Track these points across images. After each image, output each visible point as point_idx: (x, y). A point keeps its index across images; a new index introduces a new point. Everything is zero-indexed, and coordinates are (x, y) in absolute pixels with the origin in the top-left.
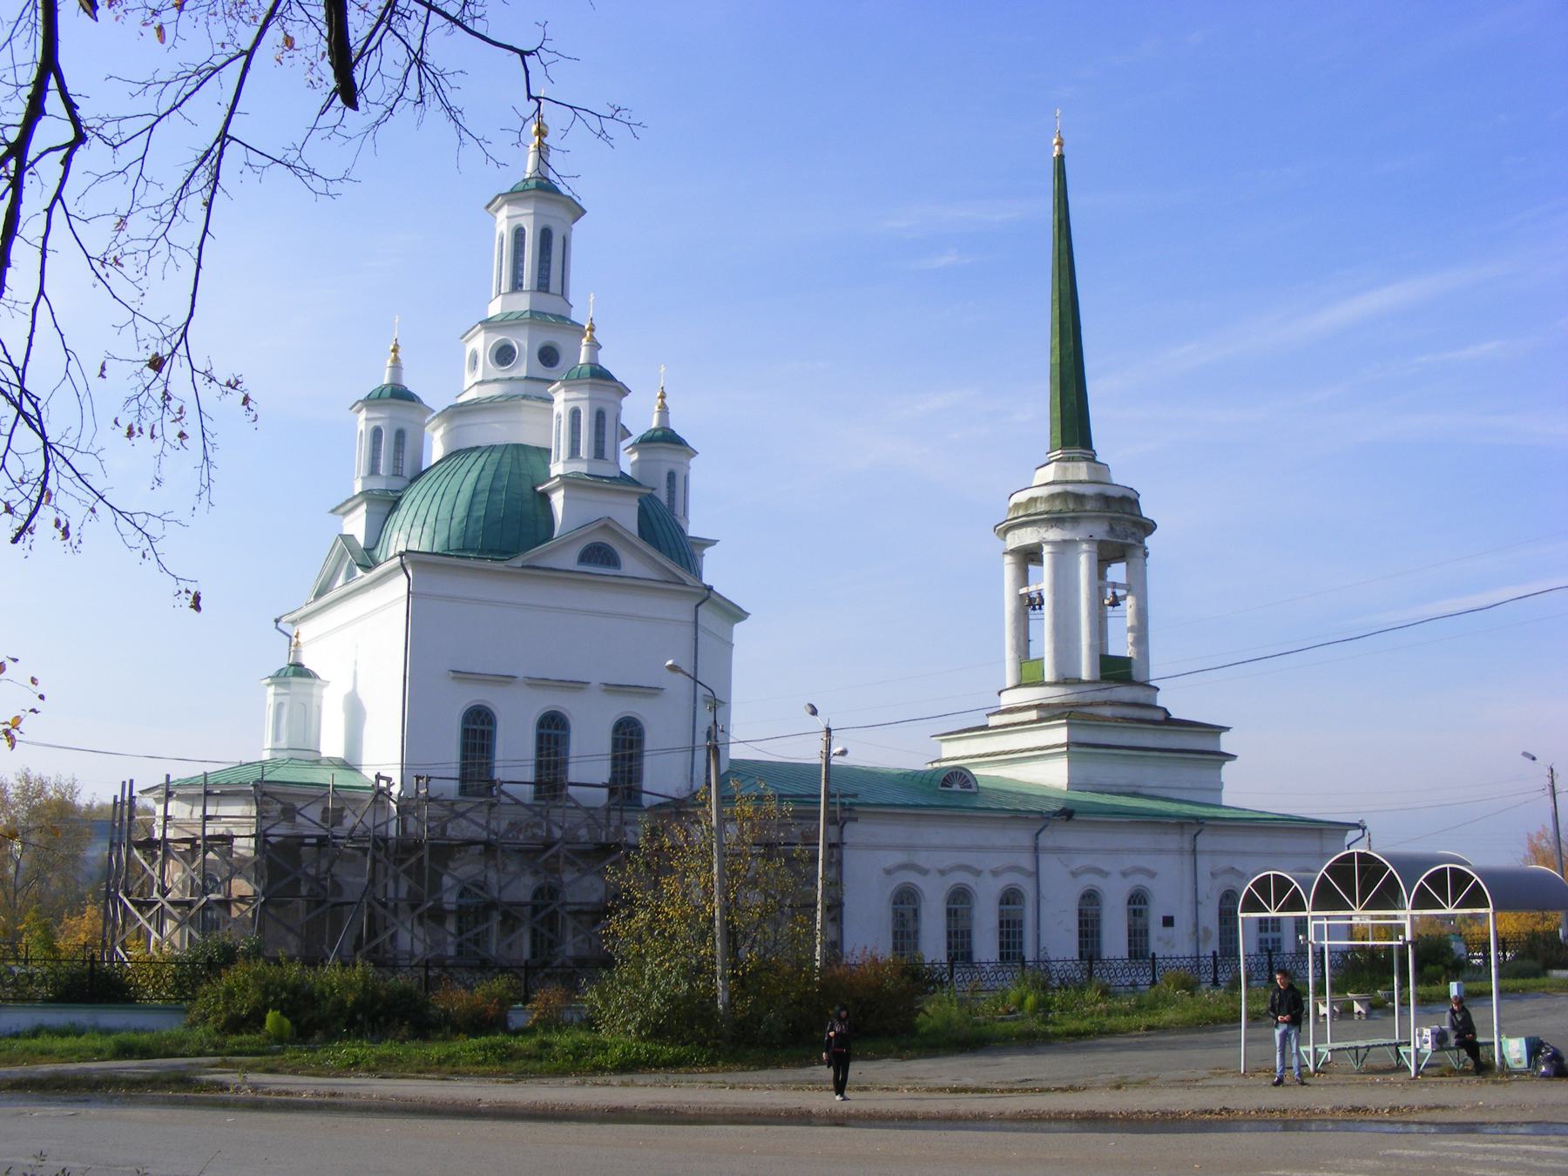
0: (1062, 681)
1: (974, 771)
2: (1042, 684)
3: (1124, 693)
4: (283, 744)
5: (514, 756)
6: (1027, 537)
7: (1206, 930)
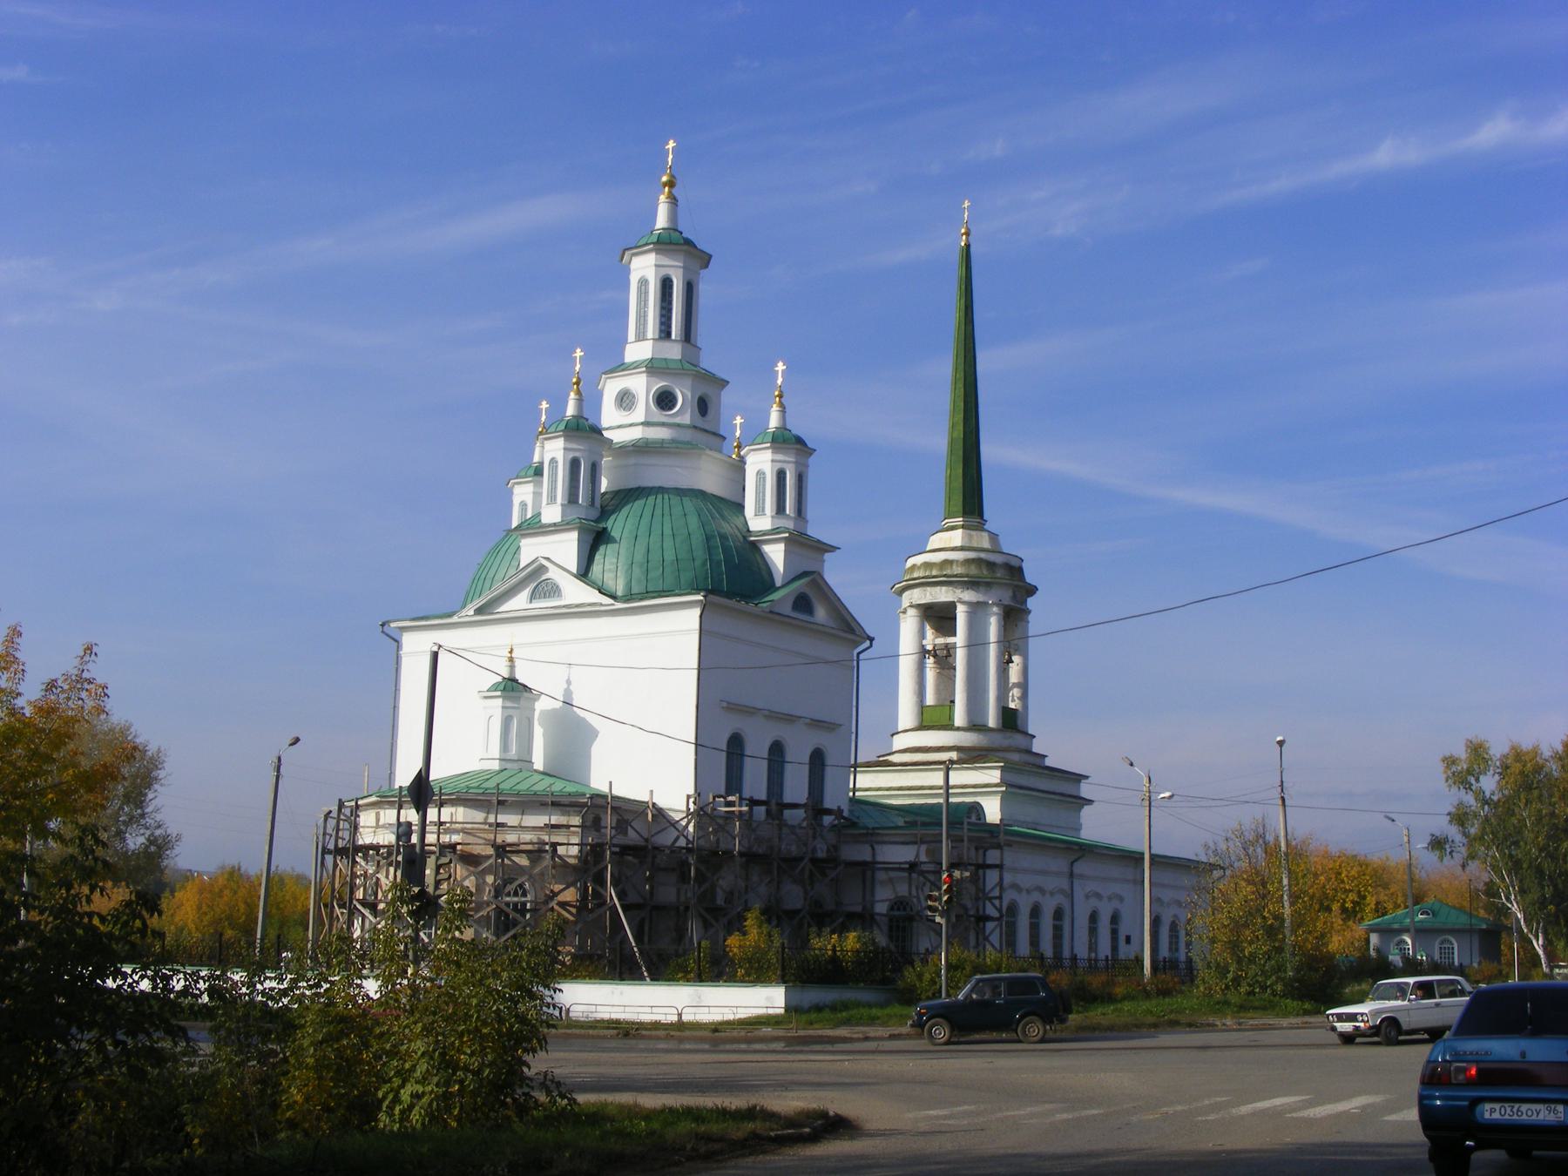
1: (535, 788)
2: (949, 726)
3: (1018, 740)
5: (755, 780)
6: (942, 595)
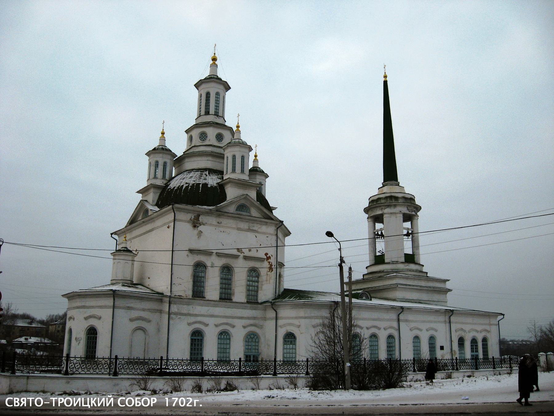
3: (412, 266)
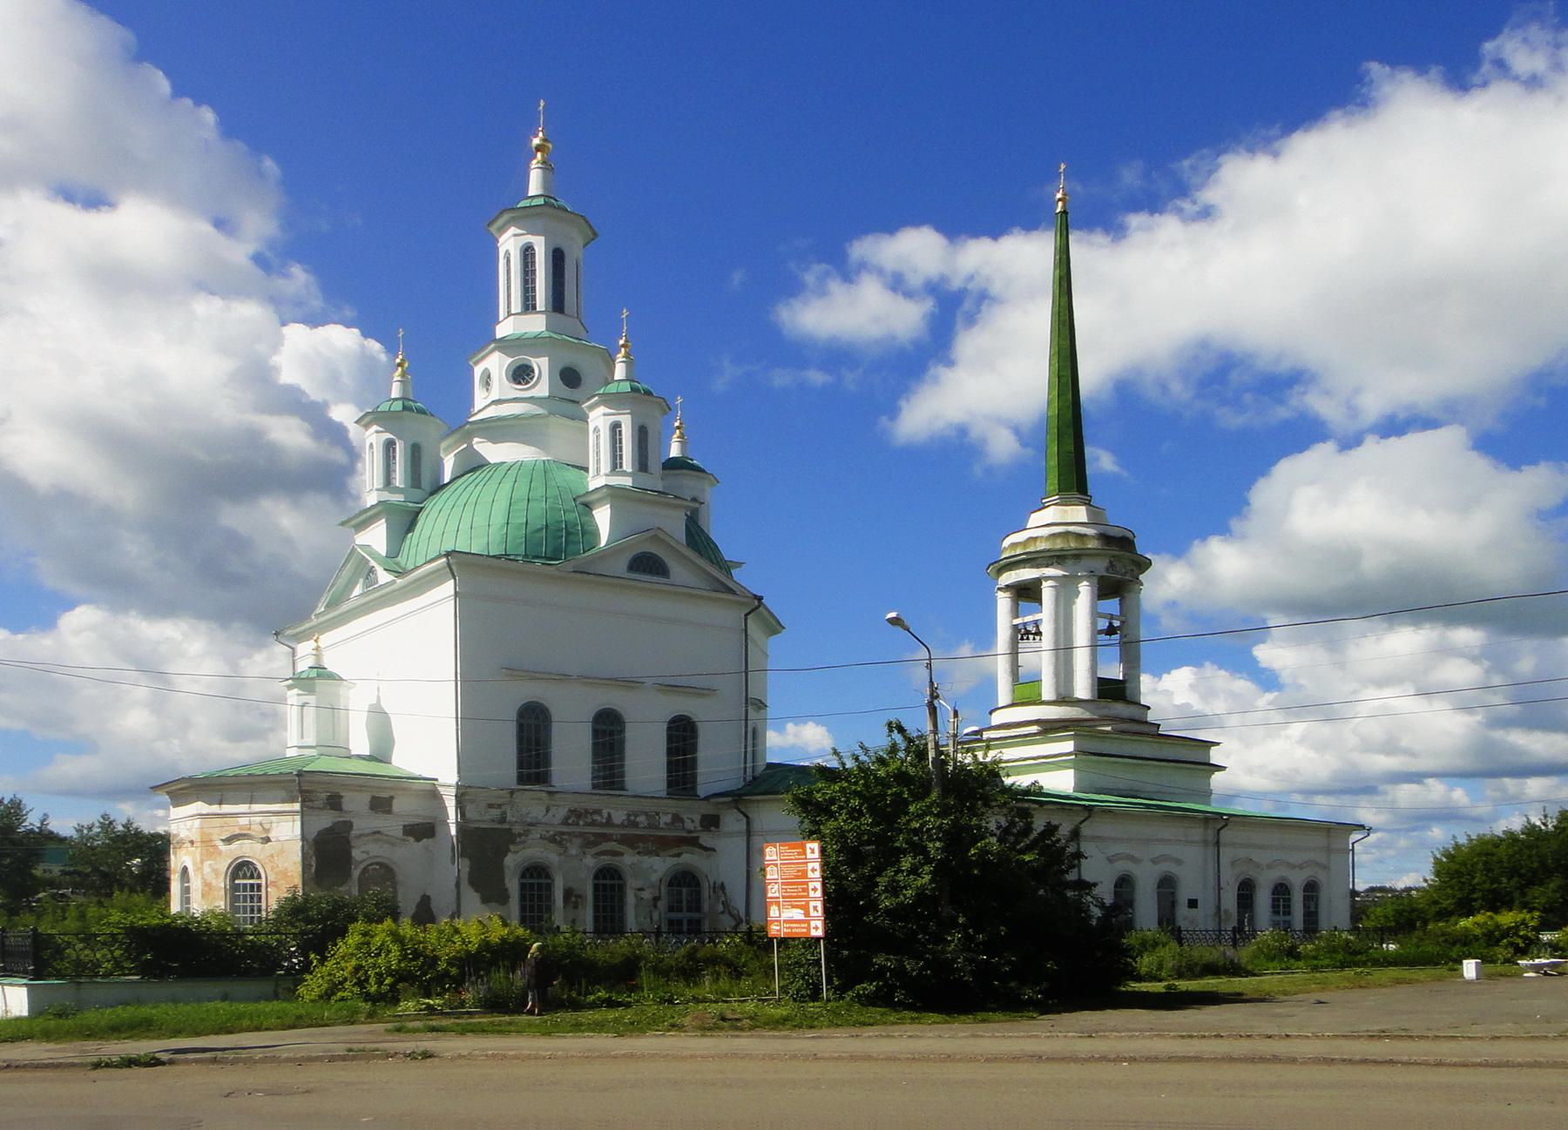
0: (1064, 699)
3: (1119, 708)
4: (310, 740)
7: (1226, 911)
